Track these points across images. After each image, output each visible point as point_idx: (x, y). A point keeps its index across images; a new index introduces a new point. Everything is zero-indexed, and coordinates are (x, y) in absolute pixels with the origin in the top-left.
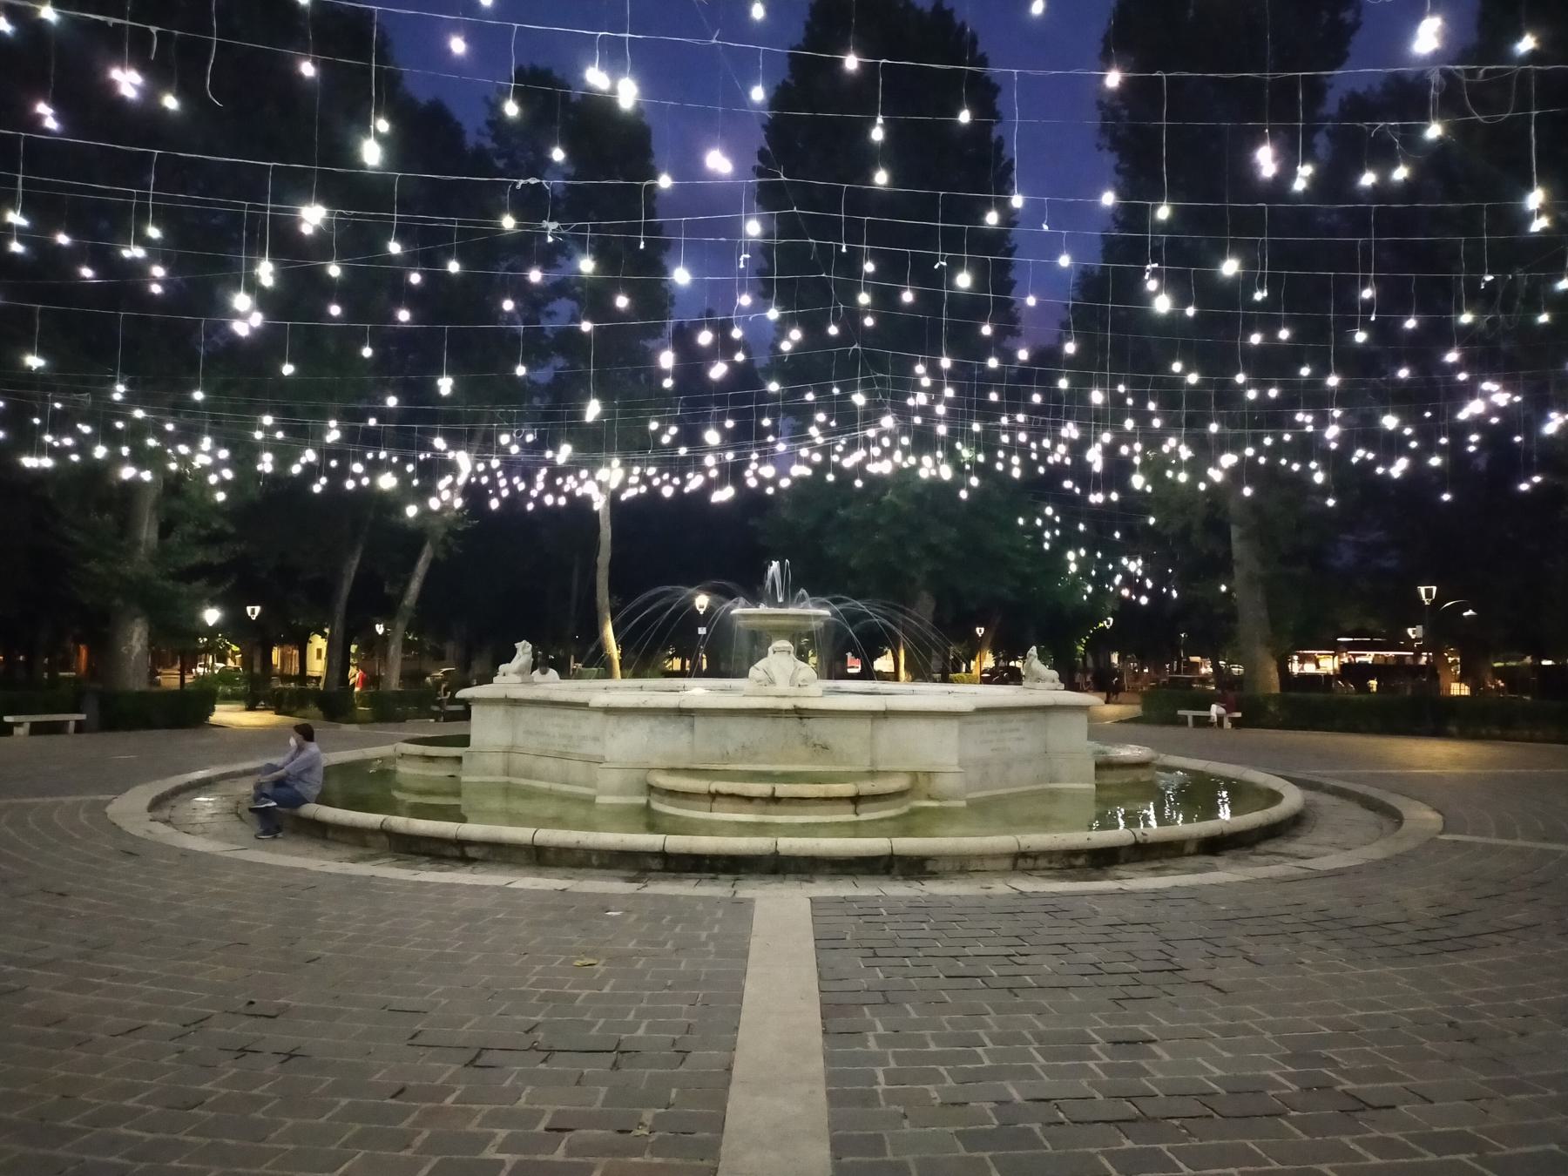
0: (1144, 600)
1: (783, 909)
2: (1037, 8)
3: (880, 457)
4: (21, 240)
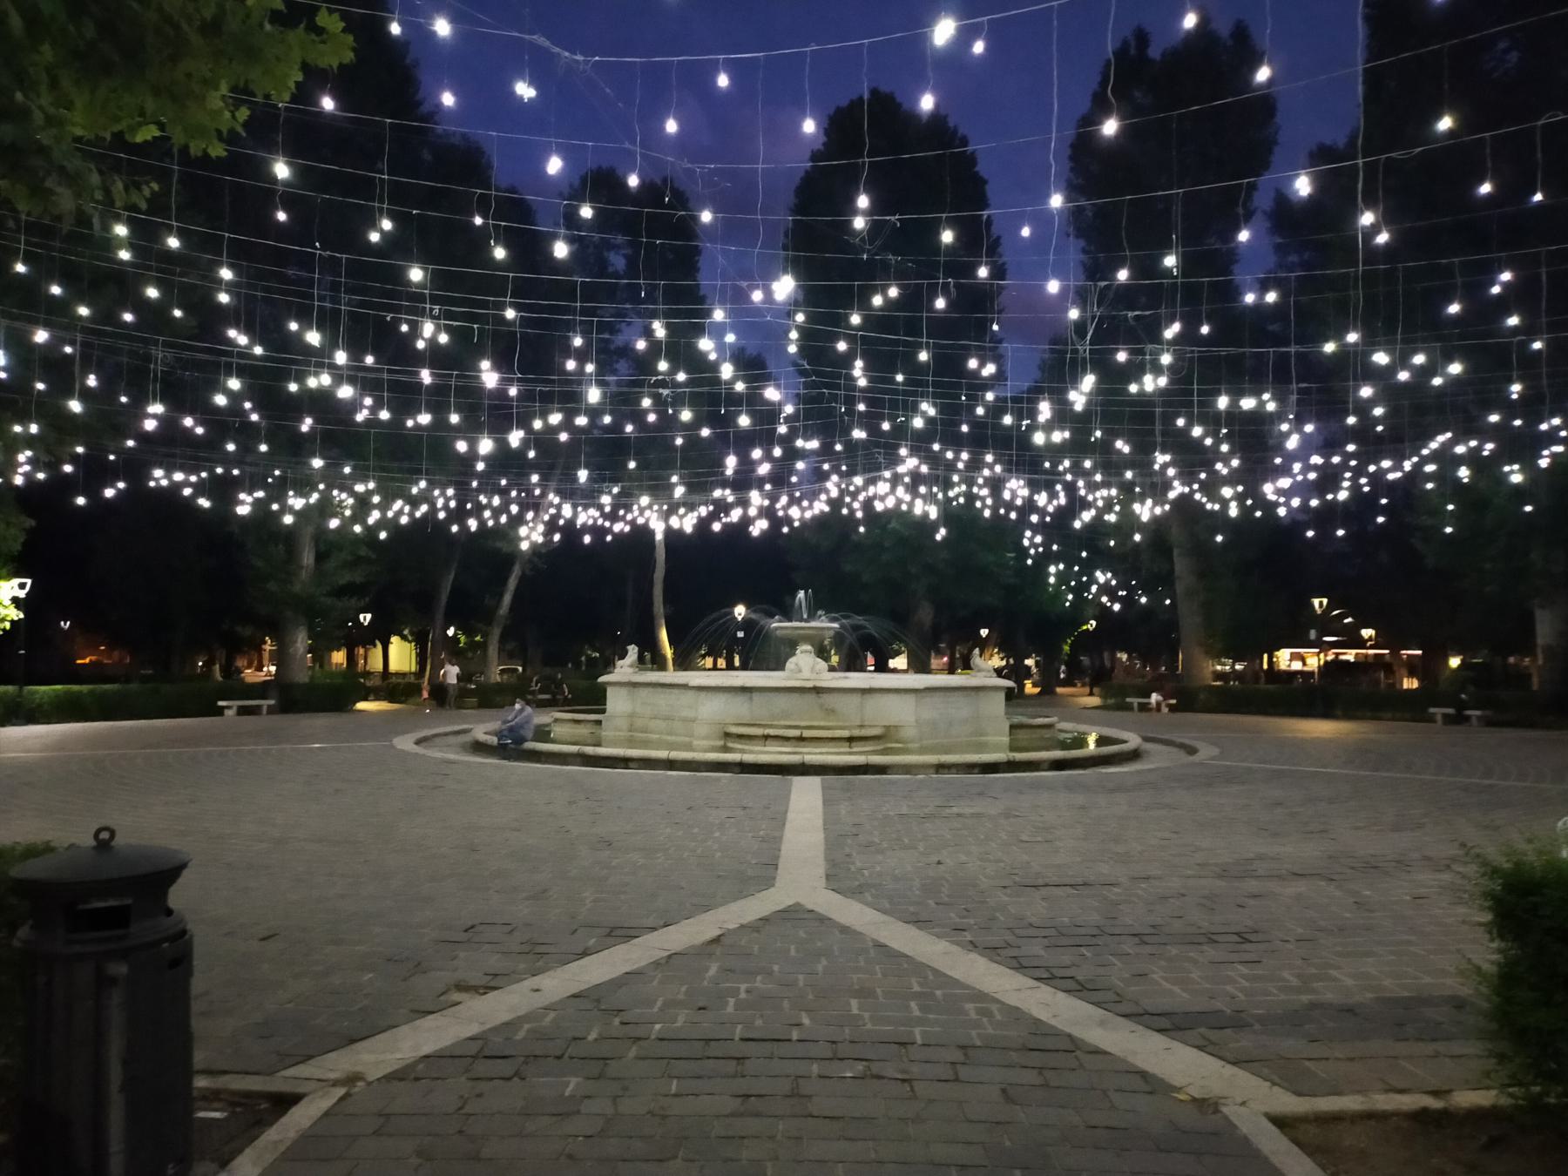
0: (1117, 607)
1: (806, 795)
3: (886, 495)
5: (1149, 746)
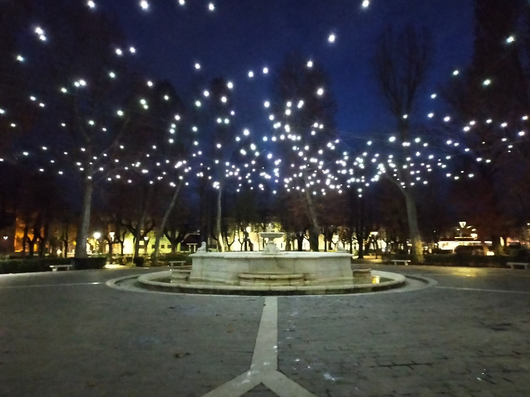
1: (271, 302)
2: (366, 4)
4: (412, 163)
5: (408, 280)
